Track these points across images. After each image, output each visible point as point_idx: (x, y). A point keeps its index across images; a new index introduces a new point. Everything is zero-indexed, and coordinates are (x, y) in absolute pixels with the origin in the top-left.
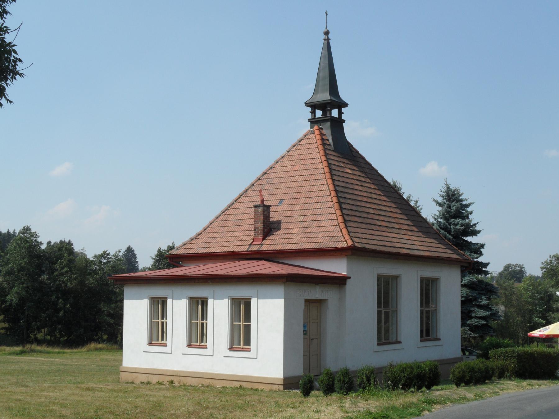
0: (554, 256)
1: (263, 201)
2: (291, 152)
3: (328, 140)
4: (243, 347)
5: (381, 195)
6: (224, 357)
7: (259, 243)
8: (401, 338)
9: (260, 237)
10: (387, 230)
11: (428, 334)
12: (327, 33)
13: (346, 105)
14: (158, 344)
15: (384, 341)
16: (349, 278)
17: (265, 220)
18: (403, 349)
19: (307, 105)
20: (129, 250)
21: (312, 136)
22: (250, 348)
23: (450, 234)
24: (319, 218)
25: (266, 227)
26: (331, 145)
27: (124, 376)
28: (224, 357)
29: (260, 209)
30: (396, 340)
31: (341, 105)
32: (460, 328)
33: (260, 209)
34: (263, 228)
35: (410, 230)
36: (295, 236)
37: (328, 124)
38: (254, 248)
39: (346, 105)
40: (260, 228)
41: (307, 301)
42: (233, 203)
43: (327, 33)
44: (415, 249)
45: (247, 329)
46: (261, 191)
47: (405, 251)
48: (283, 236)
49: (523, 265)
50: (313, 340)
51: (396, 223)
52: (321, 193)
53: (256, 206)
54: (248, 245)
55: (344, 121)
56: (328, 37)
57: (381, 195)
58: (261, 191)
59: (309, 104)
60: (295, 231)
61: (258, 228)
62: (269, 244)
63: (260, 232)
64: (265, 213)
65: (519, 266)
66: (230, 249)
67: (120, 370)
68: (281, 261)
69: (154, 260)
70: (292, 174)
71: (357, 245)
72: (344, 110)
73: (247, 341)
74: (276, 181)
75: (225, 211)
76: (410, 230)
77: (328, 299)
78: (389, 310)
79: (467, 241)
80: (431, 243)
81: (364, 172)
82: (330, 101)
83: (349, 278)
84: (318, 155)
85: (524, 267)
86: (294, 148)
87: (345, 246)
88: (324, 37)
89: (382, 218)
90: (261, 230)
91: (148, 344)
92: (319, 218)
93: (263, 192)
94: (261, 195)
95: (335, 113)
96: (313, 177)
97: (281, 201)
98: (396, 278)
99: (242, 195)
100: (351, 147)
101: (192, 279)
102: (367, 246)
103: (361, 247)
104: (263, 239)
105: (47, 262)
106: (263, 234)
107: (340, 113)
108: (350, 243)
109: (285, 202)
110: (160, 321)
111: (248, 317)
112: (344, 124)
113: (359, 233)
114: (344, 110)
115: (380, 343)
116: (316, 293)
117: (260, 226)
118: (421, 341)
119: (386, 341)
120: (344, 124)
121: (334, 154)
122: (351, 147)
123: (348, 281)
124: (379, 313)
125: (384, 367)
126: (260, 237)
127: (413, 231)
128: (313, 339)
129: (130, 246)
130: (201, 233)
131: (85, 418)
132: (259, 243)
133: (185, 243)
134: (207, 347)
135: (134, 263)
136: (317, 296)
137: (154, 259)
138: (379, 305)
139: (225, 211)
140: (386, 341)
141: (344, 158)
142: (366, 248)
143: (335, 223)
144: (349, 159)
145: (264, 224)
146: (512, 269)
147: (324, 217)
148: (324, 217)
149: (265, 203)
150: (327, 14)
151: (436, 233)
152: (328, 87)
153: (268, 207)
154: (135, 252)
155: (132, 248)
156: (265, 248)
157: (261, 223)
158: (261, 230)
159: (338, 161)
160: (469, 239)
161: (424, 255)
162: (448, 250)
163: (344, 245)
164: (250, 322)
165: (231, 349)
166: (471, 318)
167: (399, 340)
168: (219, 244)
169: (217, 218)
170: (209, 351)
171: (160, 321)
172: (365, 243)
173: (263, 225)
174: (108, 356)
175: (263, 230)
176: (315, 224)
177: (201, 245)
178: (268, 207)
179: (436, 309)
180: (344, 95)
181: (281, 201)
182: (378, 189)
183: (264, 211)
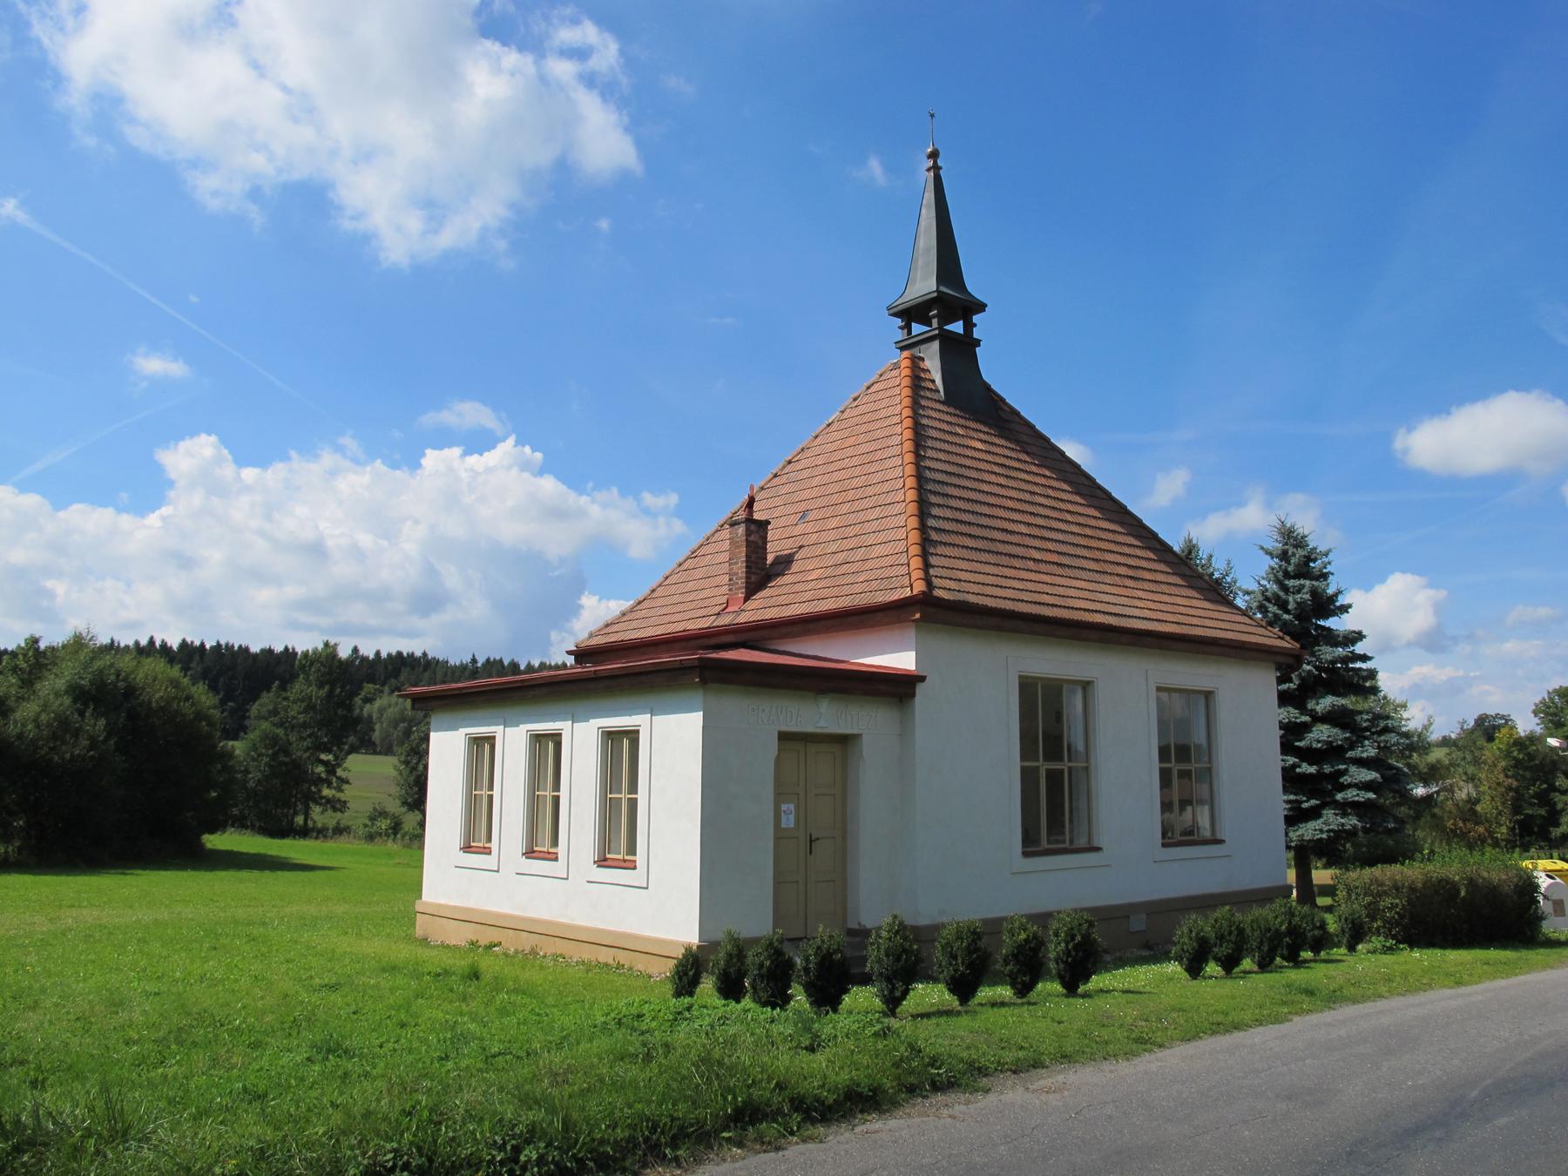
0: (1555, 691)
3: (933, 381)
4: (626, 858)
5: (1119, 533)
6: (588, 882)
7: (736, 609)
8: (1101, 840)
9: (740, 595)
10: (1060, 571)
11: (1056, 822)
13: (981, 307)
14: (480, 847)
15: (1046, 846)
16: (922, 679)
17: (754, 556)
19: (892, 311)
22: (635, 861)
23: (1287, 612)
25: (753, 570)
26: (939, 391)
27: (422, 926)
28: (588, 882)
29: (741, 530)
30: (1089, 843)
31: (969, 308)
33: (741, 529)
34: (747, 572)
35: (1131, 578)
37: (936, 345)
39: (981, 307)
40: (740, 575)
41: (784, 737)
42: (717, 531)
44: (1132, 617)
47: (1099, 618)
48: (785, 590)
49: (1509, 716)
50: (818, 842)
51: (1093, 559)
54: (715, 615)
55: (977, 343)
56: (935, 162)
57: (1119, 533)
59: (895, 310)
61: (737, 574)
63: (741, 582)
64: (752, 538)
65: (1503, 717)
67: (417, 909)
68: (772, 647)
71: (938, 593)
72: (976, 319)
75: (699, 548)
76: (1131, 578)
77: (861, 735)
78: (1063, 767)
79: (1329, 629)
80: (1191, 607)
81: (1017, 442)
82: (935, 294)
83: (922, 679)
85: (1511, 720)
87: (908, 595)
89: (1050, 546)
90: (741, 578)
91: (461, 849)
95: (957, 327)
96: (879, 455)
97: (804, 513)
99: (736, 513)
100: (1000, 403)
101: (528, 687)
103: (952, 598)
104: (746, 599)
106: (747, 588)
107: (969, 326)
109: (812, 516)
110: (624, 796)
112: (977, 349)
113: (962, 570)
114: (976, 319)
115: (1031, 844)
116: (822, 716)
117: (740, 568)
118: (1164, 845)
119: (1184, 838)
120: (977, 349)
121: (944, 408)
122: (1000, 403)
123: (920, 689)
124: (1028, 776)
125: (1011, 920)
126: (740, 595)
127: (1142, 579)
128: (818, 839)
130: (645, 599)
133: (609, 622)
134: (557, 858)
136: (822, 723)
138: (1027, 751)
139: (699, 548)
140: (1184, 838)
141: (1002, 437)
142: (968, 602)
144: (1054, 468)
145: (749, 564)
146: (1489, 722)
149: (756, 516)
150: (932, 116)
151: (1209, 587)
153: (764, 525)
156: (742, 618)
157: (742, 562)
158: (741, 578)
159: (951, 423)
160: (1332, 623)
161: (1157, 629)
162: (1206, 603)
163: (907, 593)
164: (559, 791)
166: (1343, 788)
167: (1219, 837)
169: (680, 565)
172: (973, 593)
173: (747, 567)
175: (747, 578)
178: (764, 525)
179: (1209, 766)
180: (975, 284)
181: (804, 513)
182: (1072, 492)
183: (748, 533)
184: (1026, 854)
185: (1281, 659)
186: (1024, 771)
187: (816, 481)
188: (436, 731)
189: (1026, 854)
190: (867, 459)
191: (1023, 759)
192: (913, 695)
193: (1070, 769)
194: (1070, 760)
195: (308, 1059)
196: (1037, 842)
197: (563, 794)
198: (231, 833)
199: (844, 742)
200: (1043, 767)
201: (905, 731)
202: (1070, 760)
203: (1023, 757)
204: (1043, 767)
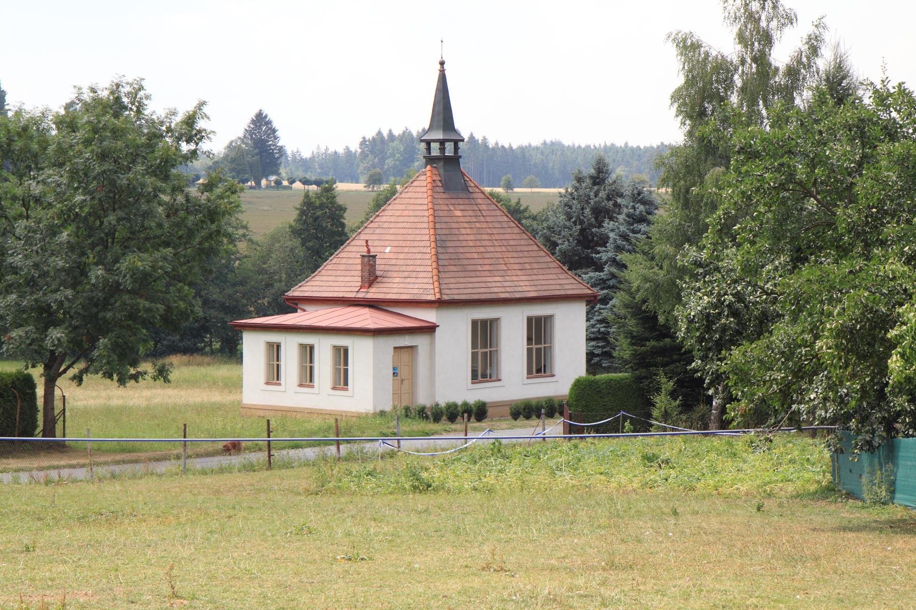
1: (369, 251)
2: (403, 194)
12: (442, 63)
18: (185, 425)
20: (260, 120)
21: (423, 177)
24: (419, 269)
32: (470, 380)
36: (396, 285)
38: (361, 295)
41: (395, 348)
43: (442, 63)
45: (346, 371)
46: (367, 241)
52: (423, 244)
53: (363, 256)
58: (367, 241)
60: (397, 280)
62: (374, 293)
66: (340, 295)
68: (385, 308)
69: (298, 212)
70: (401, 219)
73: (346, 383)
74: (386, 225)
84: (426, 201)
86: (406, 190)
88: (439, 66)
92: (419, 269)
93: (369, 243)
94: (367, 246)
98: (497, 320)
102: (456, 297)
105: (112, 218)
108: (438, 296)
110: (275, 363)
111: (346, 363)
117: (366, 274)
123: (437, 329)
129: (261, 110)
131: (82, 607)
132: (365, 290)
135: (273, 150)
137: (297, 209)
143: (430, 275)
147: (421, 269)
148: (421, 269)
152: (441, 123)
153: (374, 257)
154: (275, 124)
155: (266, 117)
156: (369, 296)
163: (433, 298)
165: (334, 388)
168: (332, 289)
170: (315, 390)
171: (275, 363)
174: (222, 371)
176: (414, 274)
177: (315, 289)
184: (472, 383)
185: (587, 299)
186: (473, 353)
187: (392, 231)
188: (566, 395)
189: (472, 383)
190: (414, 225)
191: (472, 349)
192: (435, 331)
193: (490, 351)
194: (490, 347)
195: (53, 502)
196: (532, 374)
197: (350, 368)
198: (78, 379)
199: (412, 348)
200: (480, 351)
201: (432, 344)
202: (490, 347)
203: (473, 348)
204: (480, 351)
